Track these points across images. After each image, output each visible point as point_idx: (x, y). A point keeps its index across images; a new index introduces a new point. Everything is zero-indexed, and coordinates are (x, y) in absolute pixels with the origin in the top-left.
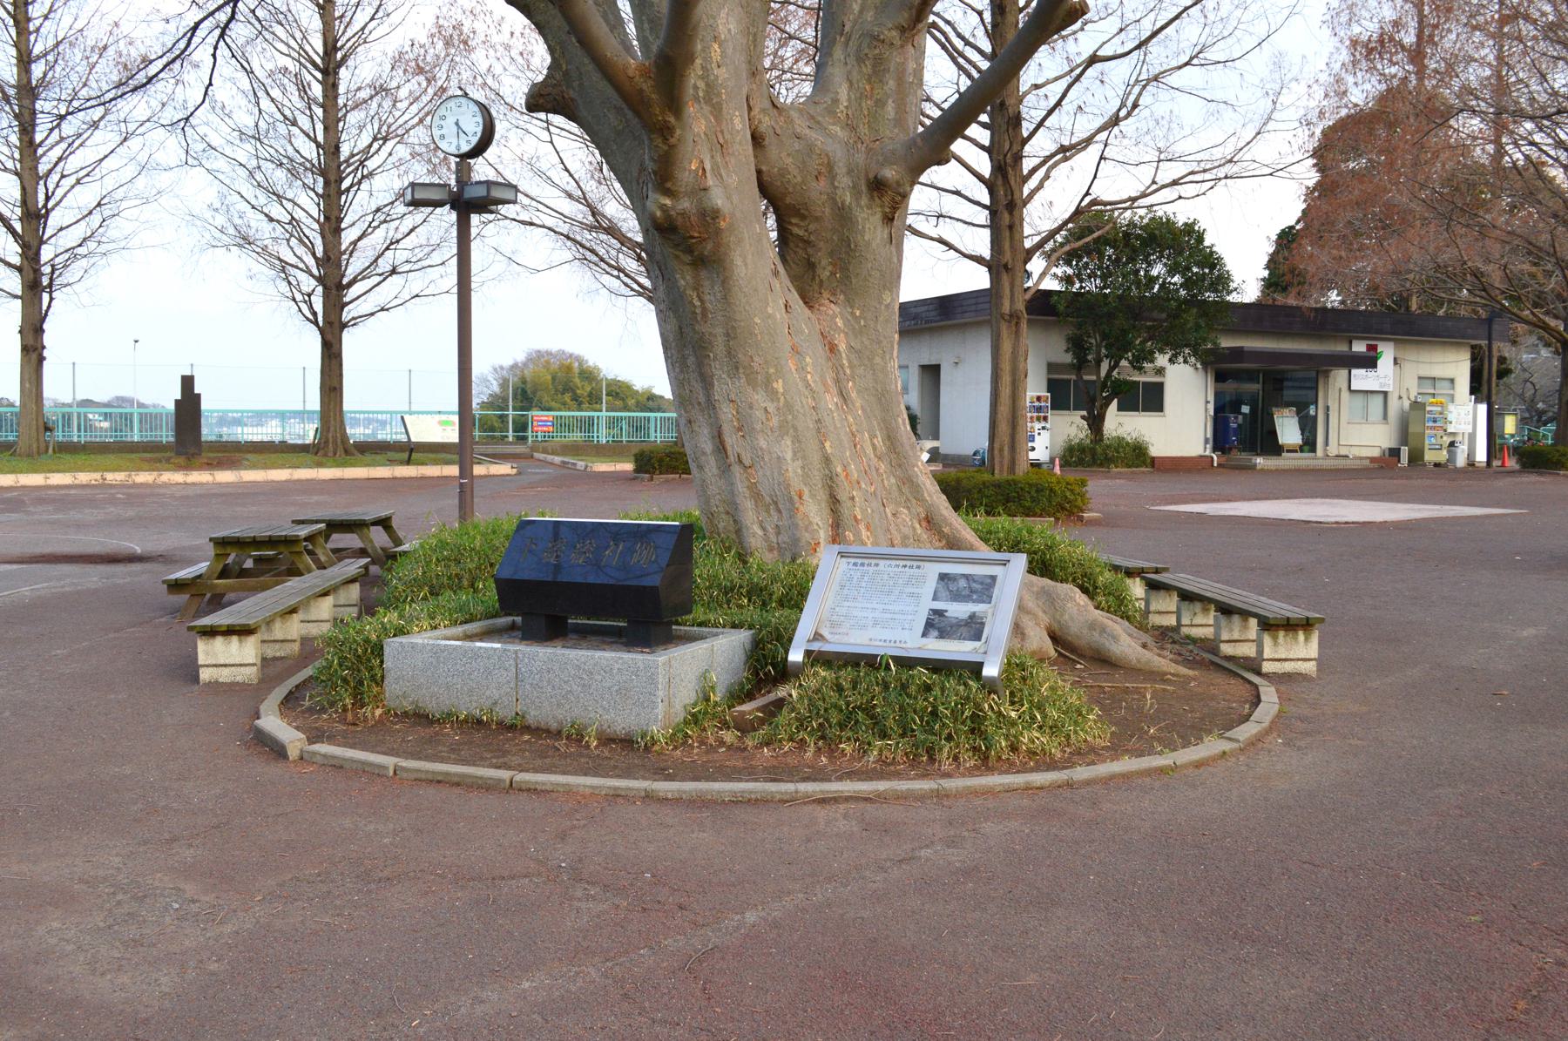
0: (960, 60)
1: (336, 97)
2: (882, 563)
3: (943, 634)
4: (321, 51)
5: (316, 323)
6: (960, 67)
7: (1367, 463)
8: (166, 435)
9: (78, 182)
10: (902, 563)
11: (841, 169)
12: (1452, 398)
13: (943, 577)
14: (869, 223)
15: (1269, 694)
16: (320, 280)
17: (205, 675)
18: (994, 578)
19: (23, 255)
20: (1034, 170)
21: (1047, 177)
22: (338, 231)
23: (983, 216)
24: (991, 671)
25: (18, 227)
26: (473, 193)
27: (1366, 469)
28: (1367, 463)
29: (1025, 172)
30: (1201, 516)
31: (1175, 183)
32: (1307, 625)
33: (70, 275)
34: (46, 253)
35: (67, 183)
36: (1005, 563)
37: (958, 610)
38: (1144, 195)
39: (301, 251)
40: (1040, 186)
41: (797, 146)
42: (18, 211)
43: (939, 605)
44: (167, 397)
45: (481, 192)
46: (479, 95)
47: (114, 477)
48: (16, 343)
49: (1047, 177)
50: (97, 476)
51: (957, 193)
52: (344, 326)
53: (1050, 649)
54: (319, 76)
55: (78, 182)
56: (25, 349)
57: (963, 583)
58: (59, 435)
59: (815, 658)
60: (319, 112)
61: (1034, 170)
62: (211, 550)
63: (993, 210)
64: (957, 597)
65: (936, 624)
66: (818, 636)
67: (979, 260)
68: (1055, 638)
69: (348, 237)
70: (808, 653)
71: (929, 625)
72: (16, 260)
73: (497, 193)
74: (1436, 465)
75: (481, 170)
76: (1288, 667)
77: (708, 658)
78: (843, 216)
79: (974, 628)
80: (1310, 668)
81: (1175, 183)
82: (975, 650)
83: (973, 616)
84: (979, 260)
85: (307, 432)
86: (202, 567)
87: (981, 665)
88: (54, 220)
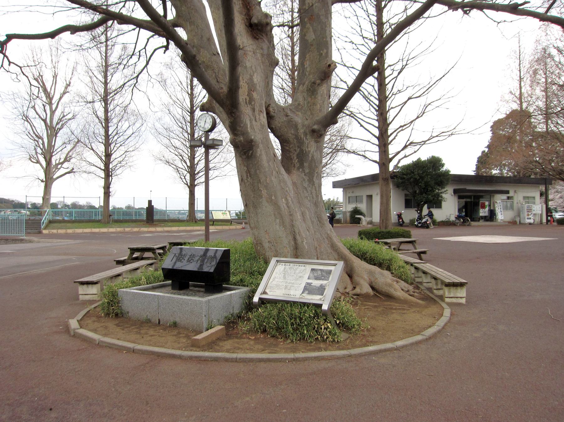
0: (371, 103)
1: (194, 120)
2: (291, 264)
3: (310, 293)
4: (189, 106)
5: (187, 184)
6: (370, 104)
7: (507, 223)
8: (144, 217)
9: (121, 145)
10: (298, 265)
11: (300, 126)
12: (534, 203)
13: (313, 270)
14: (311, 146)
15: (447, 312)
16: (188, 172)
17: (81, 297)
18: (331, 271)
19: (105, 167)
20: (391, 134)
21: (396, 136)
22: (194, 158)
23: (377, 149)
24: (325, 307)
25: (104, 158)
26: (209, 143)
27: (505, 225)
28: (507, 223)
29: (389, 134)
30: (449, 241)
31: (437, 136)
32: (461, 285)
33: (118, 172)
34: (111, 166)
35: (118, 145)
36: (335, 265)
37: (317, 283)
38: (429, 140)
39: (184, 164)
40: (394, 138)
41: (285, 119)
42: (104, 154)
43: (310, 281)
44: (146, 205)
45: (211, 142)
46: (13, 68)
47: (127, 229)
48: (102, 191)
49: (396, 136)
50: (122, 229)
51: (368, 141)
52: (196, 186)
53: (370, 291)
54: (189, 114)
55: (121, 145)
56: (105, 193)
57: (319, 272)
58: (116, 217)
59: (262, 301)
60: (189, 124)
61: (391, 134)
62: (129, 252)
63: (379, 146)
64: (317, 278)
65: (308, 289)
66: (264, 293)
67: (375, 162)
68: (373, 288)
69: (196, 161)
70: (260, 299)
71: (305, 289)
72: (103, 168)
73: (216, 143)
74: (530, 224)
75: (212, 136)
76: (454, 300)
77: (231, 298)
78: (300, 143)
79: (321, 290)
80: (463, 301)
81: (437, 136)
82: (320, 299)
83: (321, 285)
84: (375, 162)
85: (185, 217)
86: (126, 258)
87: (322, 305)
88: (113, 157)
